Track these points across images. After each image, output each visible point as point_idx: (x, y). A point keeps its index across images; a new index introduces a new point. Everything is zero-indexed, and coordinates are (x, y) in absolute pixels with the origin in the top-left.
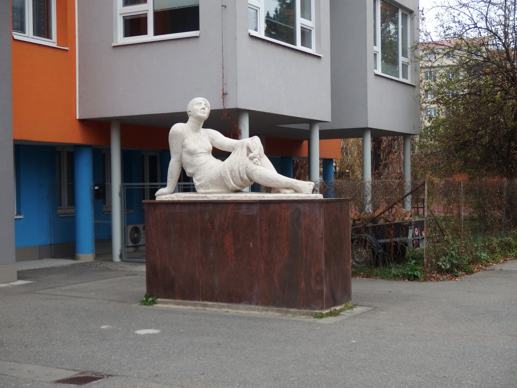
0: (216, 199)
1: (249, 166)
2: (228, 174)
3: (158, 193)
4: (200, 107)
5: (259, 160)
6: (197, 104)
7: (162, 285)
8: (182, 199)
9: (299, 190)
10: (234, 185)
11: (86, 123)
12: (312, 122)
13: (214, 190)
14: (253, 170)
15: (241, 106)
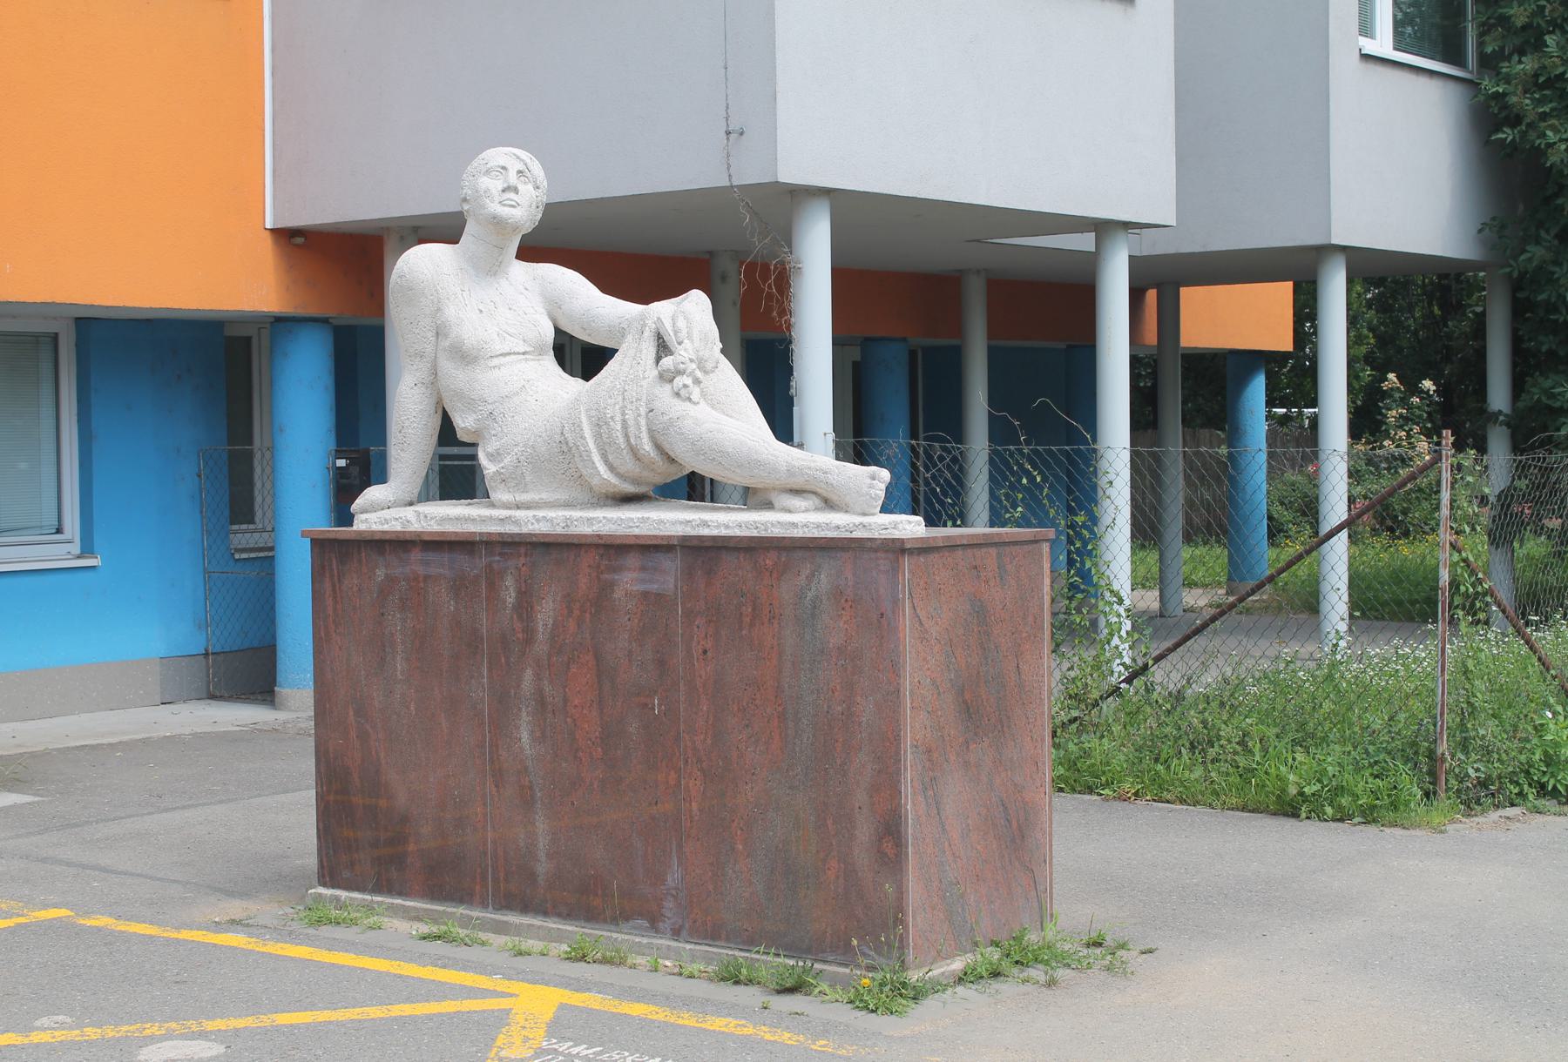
0: (542, 528)
1: (657, 405)
2: (588, 433)
3: (359, 502)
4: (512, 183)
5: (697, 381)
6: (488, 172)
7: (371, 844)
8: (436, 528)
9: (834, 498)
10: (614, 480)
11: (300, 240)
12: (1104, 228)
13: (544, 496)
14: (671, 423)
15: (790, 174)
